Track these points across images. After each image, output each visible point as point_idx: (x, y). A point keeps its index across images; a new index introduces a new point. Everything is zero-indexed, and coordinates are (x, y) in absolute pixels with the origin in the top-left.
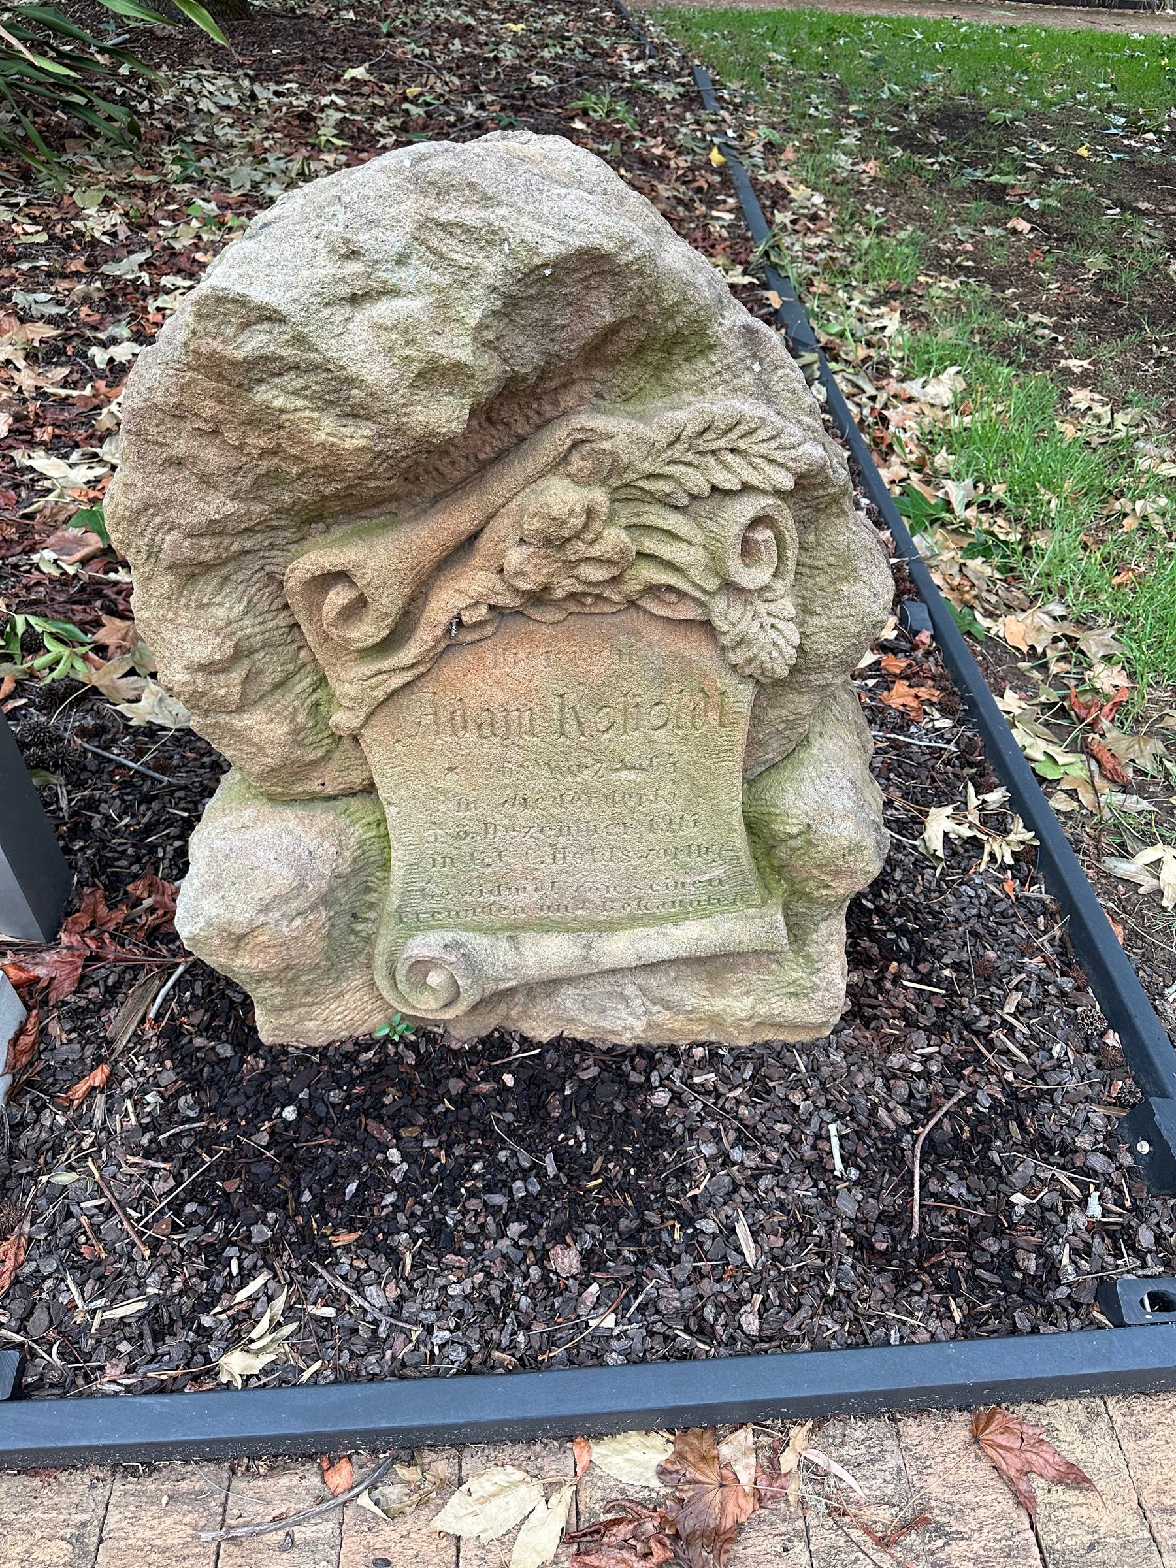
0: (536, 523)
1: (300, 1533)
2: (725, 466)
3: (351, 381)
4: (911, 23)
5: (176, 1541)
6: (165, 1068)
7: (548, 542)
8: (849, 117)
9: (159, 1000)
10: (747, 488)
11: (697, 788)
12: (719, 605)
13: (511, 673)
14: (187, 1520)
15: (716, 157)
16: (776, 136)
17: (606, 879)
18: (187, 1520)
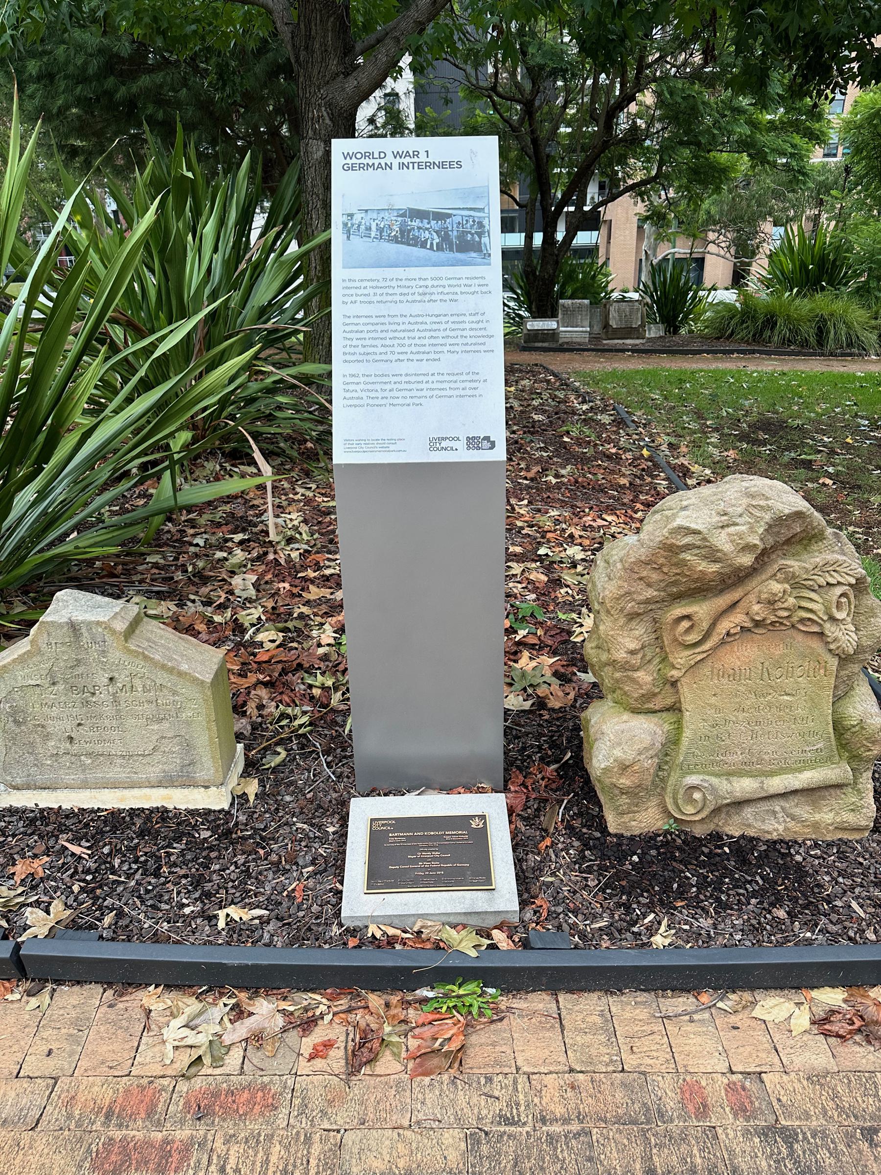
0: (766, 596)
1: (696, 1017)
2: (832, 576)
3: (718, 551)
4: (725, 373)
7: (769, 602)
8: (708, 427)
10: (839, 583)
11: (814, 703)
12: (827, 625)
13: (746, 654)
15: (645, 452)
16: (673, 440)
17: (772, 748)
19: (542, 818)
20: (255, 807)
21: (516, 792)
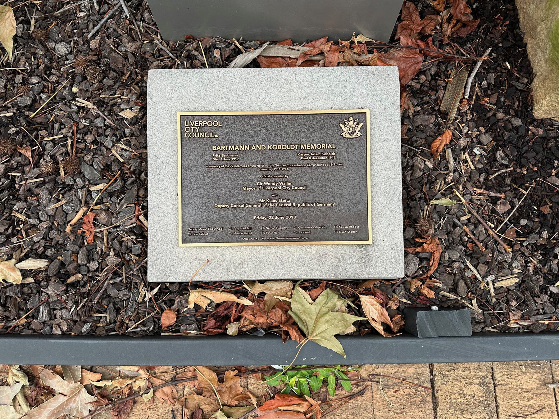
5: (533, 387)
6: (481, 132)
9: (469, 86)
14: (535, 376)
18: (535, 376)
19: (441, 93)
20: (17, 61)
21: (408, 47)
